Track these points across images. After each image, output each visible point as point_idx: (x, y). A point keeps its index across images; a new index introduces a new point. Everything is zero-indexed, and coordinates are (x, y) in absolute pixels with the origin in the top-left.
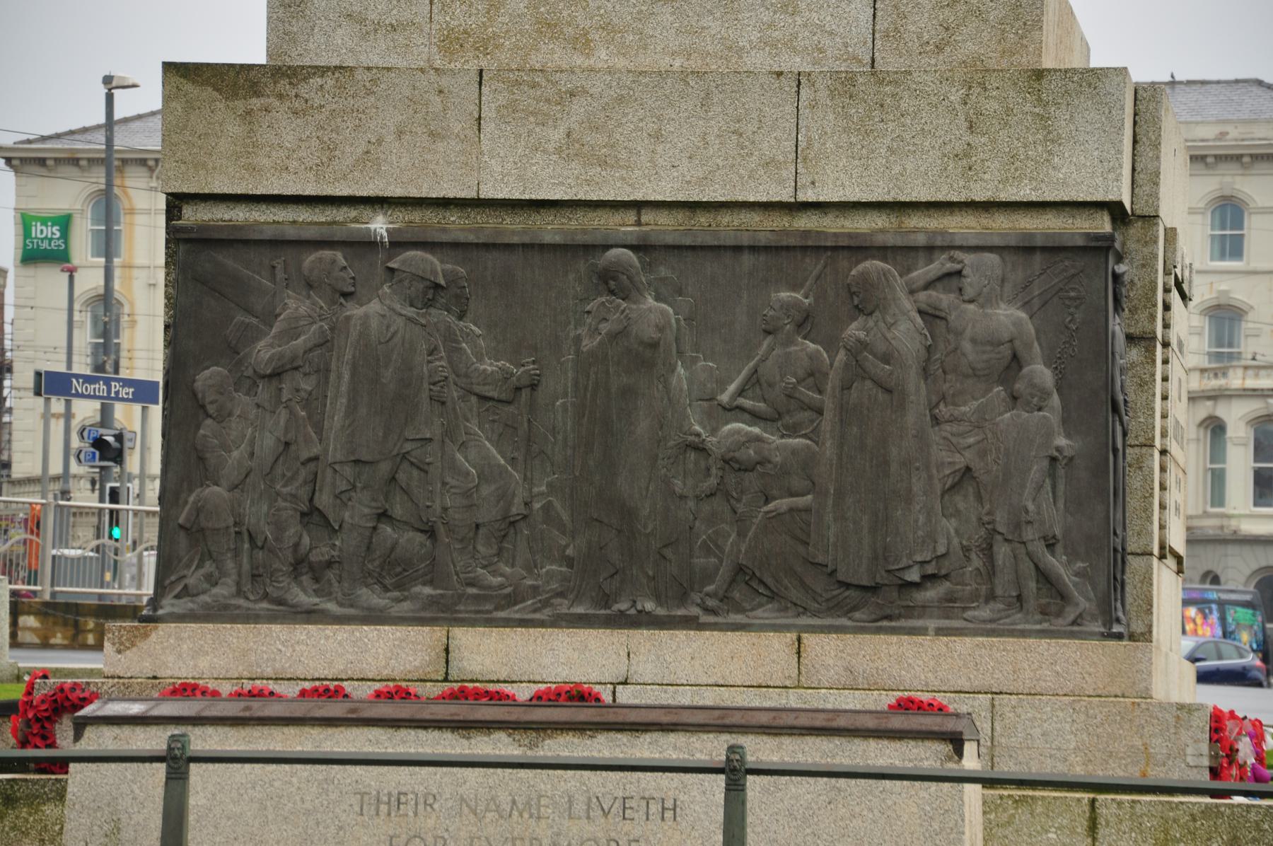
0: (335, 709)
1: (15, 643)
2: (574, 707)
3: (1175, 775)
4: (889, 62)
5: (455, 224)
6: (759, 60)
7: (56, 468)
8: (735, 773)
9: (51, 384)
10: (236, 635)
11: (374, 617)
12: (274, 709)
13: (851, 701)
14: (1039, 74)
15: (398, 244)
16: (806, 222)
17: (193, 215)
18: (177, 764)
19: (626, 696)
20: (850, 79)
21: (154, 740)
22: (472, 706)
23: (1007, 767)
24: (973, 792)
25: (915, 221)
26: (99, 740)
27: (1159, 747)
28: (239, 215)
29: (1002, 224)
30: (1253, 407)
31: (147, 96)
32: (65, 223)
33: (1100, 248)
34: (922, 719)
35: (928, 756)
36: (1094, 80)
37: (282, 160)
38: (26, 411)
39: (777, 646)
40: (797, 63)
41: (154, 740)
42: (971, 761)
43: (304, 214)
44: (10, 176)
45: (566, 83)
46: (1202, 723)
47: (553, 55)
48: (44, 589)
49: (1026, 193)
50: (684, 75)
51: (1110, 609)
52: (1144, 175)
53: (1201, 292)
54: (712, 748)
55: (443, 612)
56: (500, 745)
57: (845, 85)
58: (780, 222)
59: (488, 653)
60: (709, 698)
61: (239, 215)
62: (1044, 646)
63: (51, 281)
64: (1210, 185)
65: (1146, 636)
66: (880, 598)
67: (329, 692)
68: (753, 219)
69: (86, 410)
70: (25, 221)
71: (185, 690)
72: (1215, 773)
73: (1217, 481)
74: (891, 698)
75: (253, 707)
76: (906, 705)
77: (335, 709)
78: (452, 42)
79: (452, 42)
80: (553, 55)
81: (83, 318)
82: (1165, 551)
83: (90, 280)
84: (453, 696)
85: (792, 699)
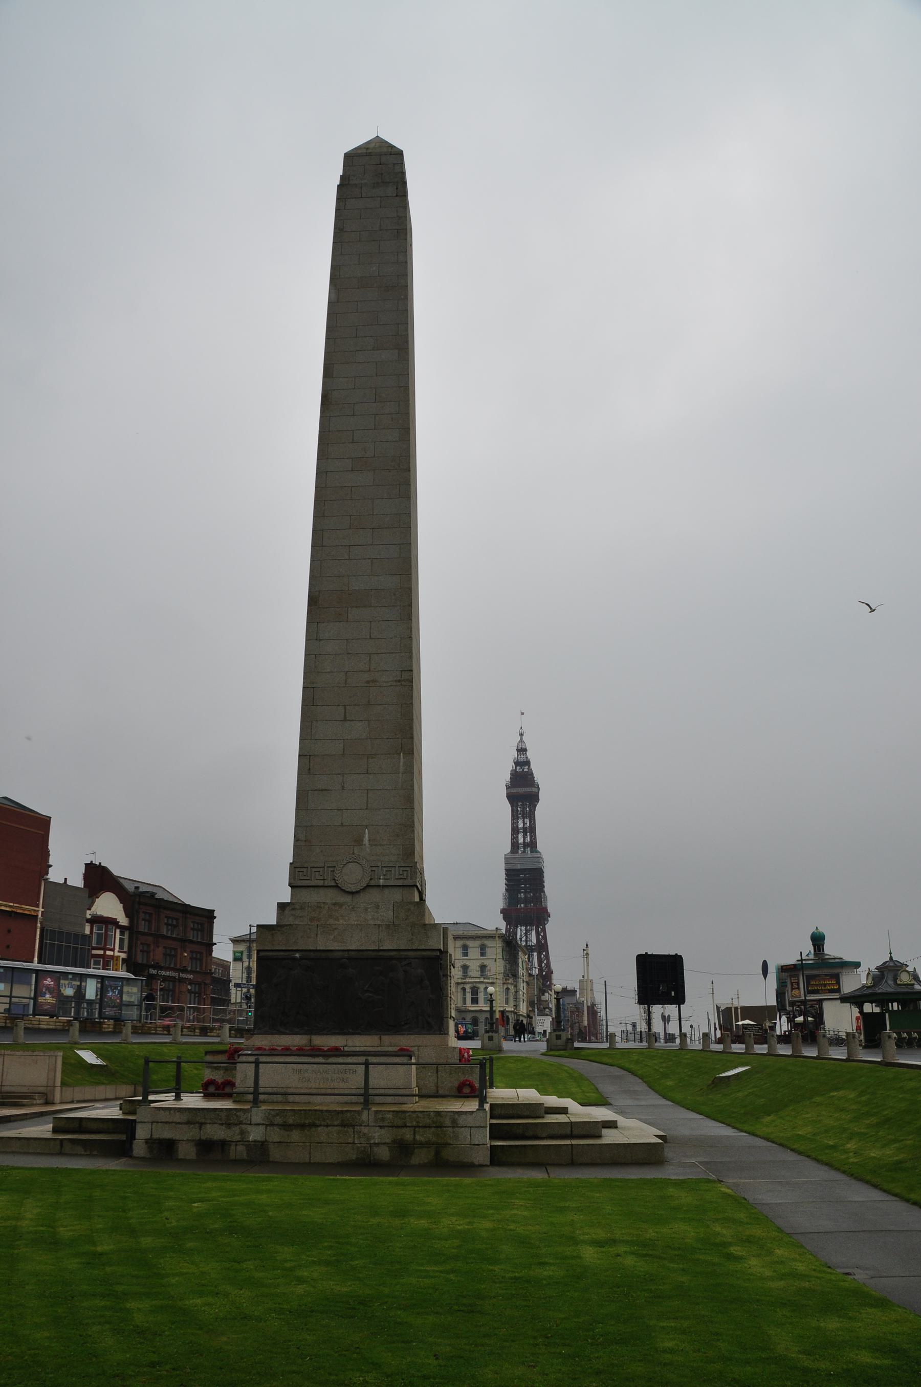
0: (288, 1052)
1: (230, 1037)
2: (336, 1052)
3: (453, 1061)
4: (397, 922)
5: (312, 955)
6: (371, 922)
7: (239, 1001)
8: (367, 1064)
9: (237, 985)
10: (269, 1037)
11: (297, 1034)
12: (276, 1053)
13: (391, 1049)
14: (425, 925)
15: (301, 959)
16: (381, 953)
17: (262, 954)
18: (257, 1063)
19: (346, 1049)
20: (389, 926)
21: (252, 1059)
22: (316, 1052)
23: (421, 1061)
24: (414, 1067)
25: (402, 953)
26: (244, 1059)
27: (450, 1056)
28: (270, 954)
29: (419, 953)
30: (471, 985)
31: (254, 930)
32: (242, 953)
33: (437, 958)
34: (405, 1053)
35: (404, 1060)
36: (436, 926)
37: (279, 943)
38: (233, 990)
39: (376, 1038)
40: (379, 923)
41: (252, 1059)
42: (413, 1061)
43: (282, 953)
44: (232, 945)
45: (334, 927)
46: (457, 1050)
47: (331, 921)
48: (235, 1026)
49: (423, 947)
50: (357, 925)
51: (442, 1030)
52: (445, 944)
53: (458, 964)
54: (362, 1059)
55: (310, 1032)
56: (321, 1060)
57: (388, 927)
58: (375, 953)
59: (321, 1041)
60: (362, 1049)
61: (270, 954)
62: (428, 1037)
63: (239, 964)
64: (459, 943)
65: (447, 1034)
66: (396, 1028)
67: (287, 1049)
68: (370, 953)
69: (245, 990)
70: (234, 952)
71: (259, 1049)
72: (460, 1060)
73: (465, 999)
74: (397, 1048)
75: (272, 1052)
76: (401, 1050)
77: (288, 1052)
78: (312, 919)
79: (312, 919)
80: (331, 921)
81: (245, 971)
82: (451, 1017)
83: (246, 964)
84: (313, 1049)
85: (379, 1049)
